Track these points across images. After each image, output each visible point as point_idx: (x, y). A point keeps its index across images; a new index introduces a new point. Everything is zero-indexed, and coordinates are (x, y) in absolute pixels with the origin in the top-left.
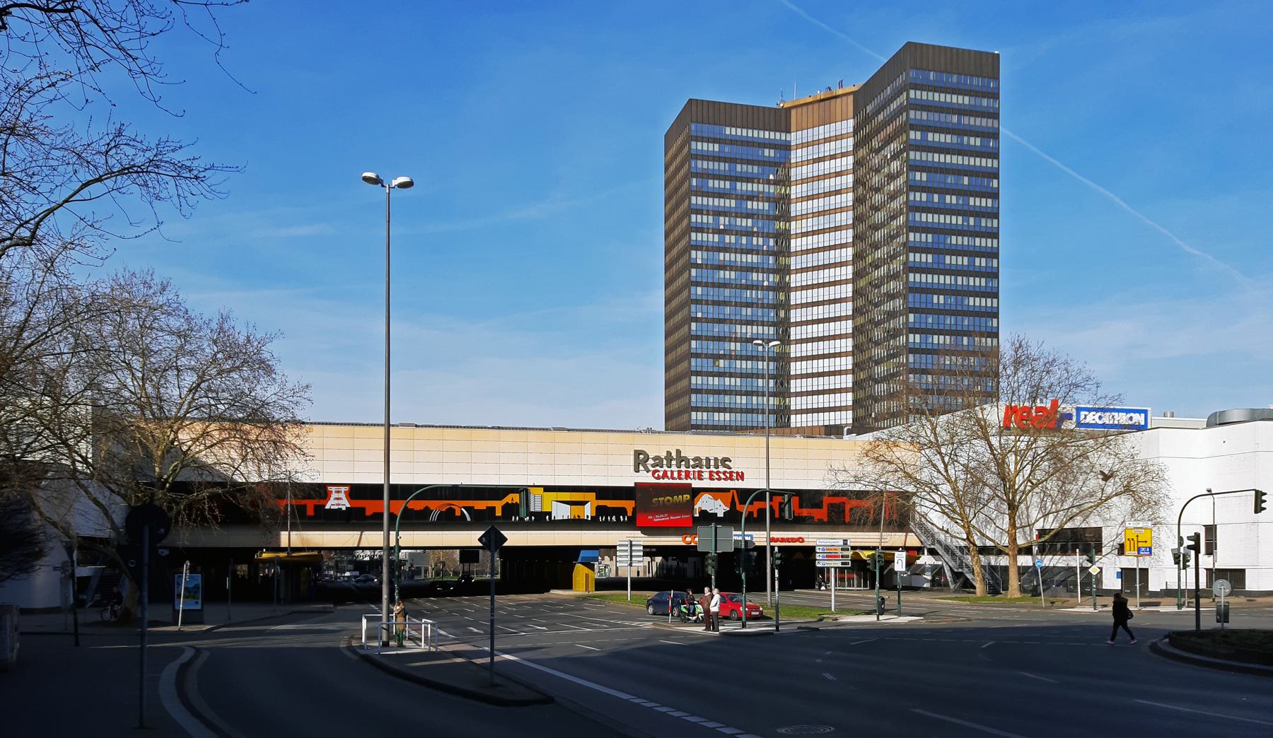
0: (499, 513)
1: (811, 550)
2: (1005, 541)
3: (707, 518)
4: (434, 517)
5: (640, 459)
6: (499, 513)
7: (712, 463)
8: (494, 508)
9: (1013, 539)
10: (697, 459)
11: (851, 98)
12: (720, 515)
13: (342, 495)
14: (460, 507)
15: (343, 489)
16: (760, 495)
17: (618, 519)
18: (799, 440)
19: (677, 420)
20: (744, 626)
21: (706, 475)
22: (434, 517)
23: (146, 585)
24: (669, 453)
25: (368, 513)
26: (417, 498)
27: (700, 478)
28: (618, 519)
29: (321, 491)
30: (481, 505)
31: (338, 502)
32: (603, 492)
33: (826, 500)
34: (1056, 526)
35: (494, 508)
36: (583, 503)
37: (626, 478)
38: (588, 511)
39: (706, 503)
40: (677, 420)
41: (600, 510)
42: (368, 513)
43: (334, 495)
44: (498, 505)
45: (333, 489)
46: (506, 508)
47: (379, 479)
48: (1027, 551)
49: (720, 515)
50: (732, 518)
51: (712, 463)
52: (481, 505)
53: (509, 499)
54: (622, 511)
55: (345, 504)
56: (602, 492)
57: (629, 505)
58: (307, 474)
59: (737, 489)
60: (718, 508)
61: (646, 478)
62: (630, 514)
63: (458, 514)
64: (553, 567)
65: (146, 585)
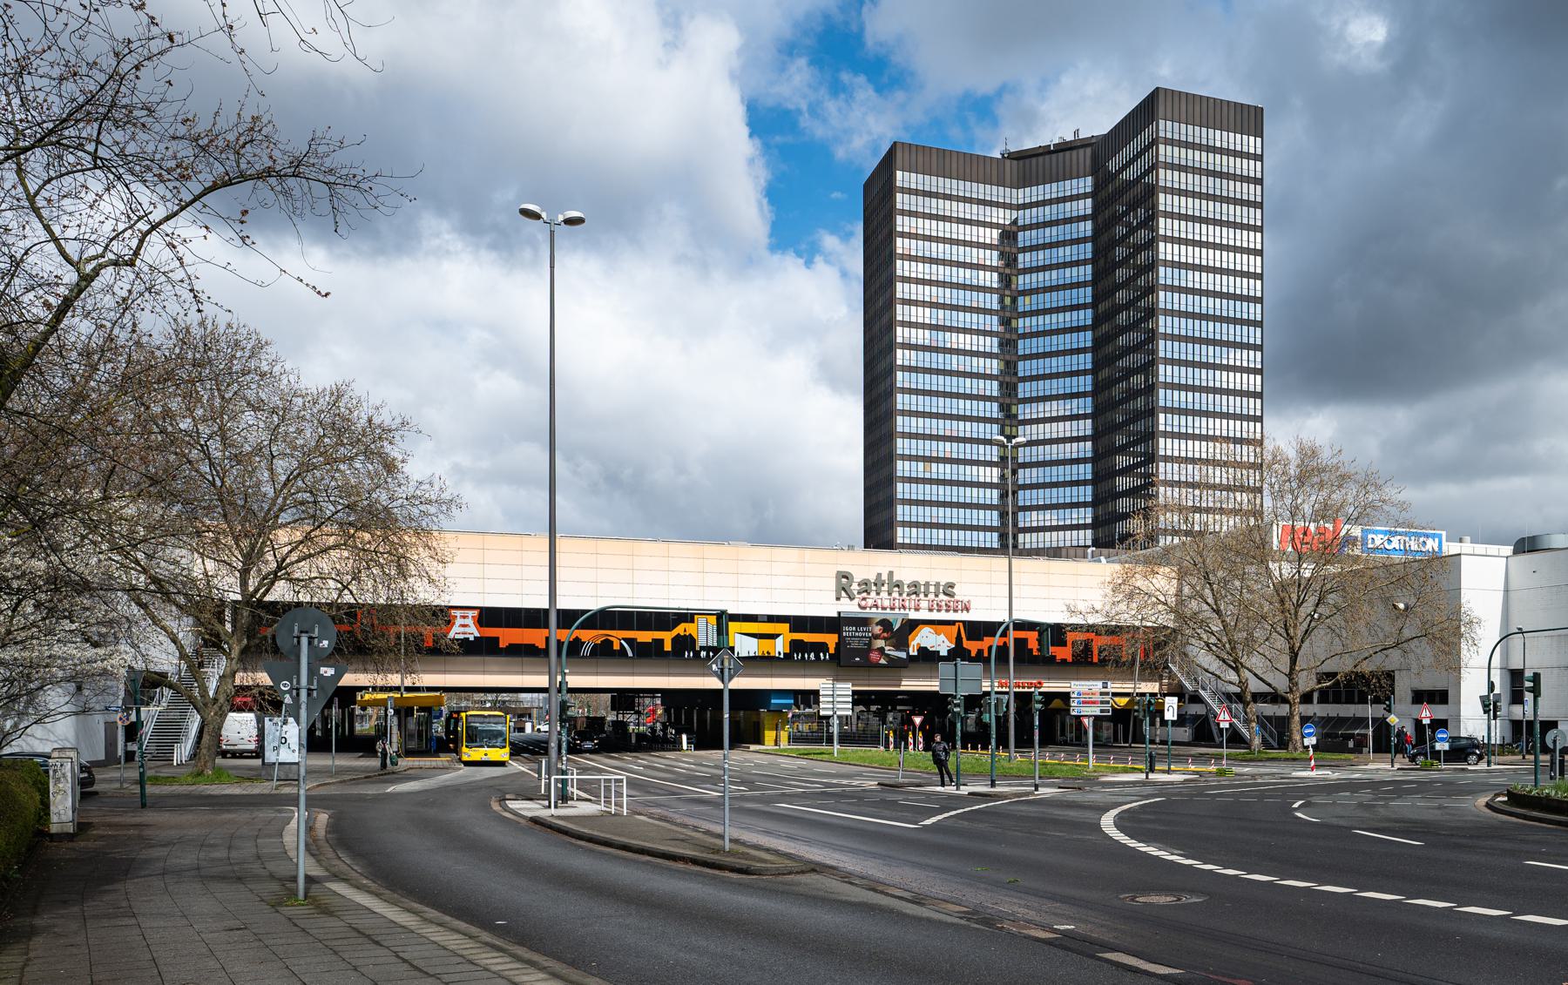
0: (668, 647)
1: (1066, 697)
2: (1281, 684)
3: (928, 657)
4: (586, 650)
5: (844, 584)
6: (668, 647)
7: (932, 589)
8: (661, 642)
9: (1293, 682)
10: (915, 585)
11: (1089, 150)
12: (944, 653)
13: (470, 621)
14: (618, 637)
15: (471, 613)
16: (989, 628)
17: (817, 657)
18: (1040, 564)
19: (879, 534)
20: (993, 785)
21: (924, 604)
22: (586, 650)
23: (963, 922)
24: (879, 575)
25: (502, 645)
26: (583, 626)
27: (917, 609)
28: (817, 657)
29: (442, 614)
30: (645, 636)
31: (465, 628)
32: (799, 623)
33: (1070, 637)
34: (1348, 668)
35: (661, 642)
36: (774, 637)
37: (826, 606)
38: (780, 647)
39: (925, 638)
40: (879, 534)
41: (796, 646)
42: (502, 645)
43: (459, 621)
44: (667, 637)
45: (458, 613)
46: (677, 640)
47: (536, 599)
48: (1307, 698)
49: (944, 653)
50: (958, 653)
51: (932, 589)
52: (645, 636)
53: (680, 629)
54: (822, 647)
55: (473, 632)
56: (798, 623)
57: (831, 640)
58: (423, 593)
59: (964, 622)
60: (940, 643)
61: (849, 607)
62: (832, 651)
63: (616, 647)
64: (748, 717)
65: (963, 922)
